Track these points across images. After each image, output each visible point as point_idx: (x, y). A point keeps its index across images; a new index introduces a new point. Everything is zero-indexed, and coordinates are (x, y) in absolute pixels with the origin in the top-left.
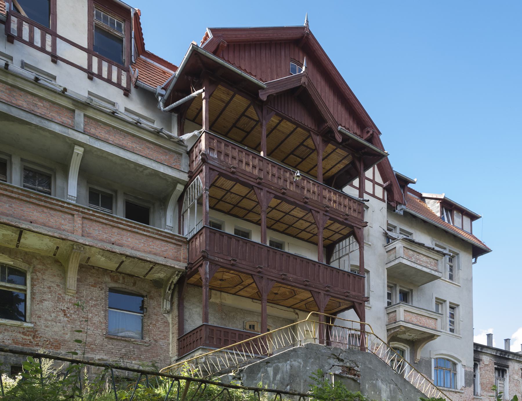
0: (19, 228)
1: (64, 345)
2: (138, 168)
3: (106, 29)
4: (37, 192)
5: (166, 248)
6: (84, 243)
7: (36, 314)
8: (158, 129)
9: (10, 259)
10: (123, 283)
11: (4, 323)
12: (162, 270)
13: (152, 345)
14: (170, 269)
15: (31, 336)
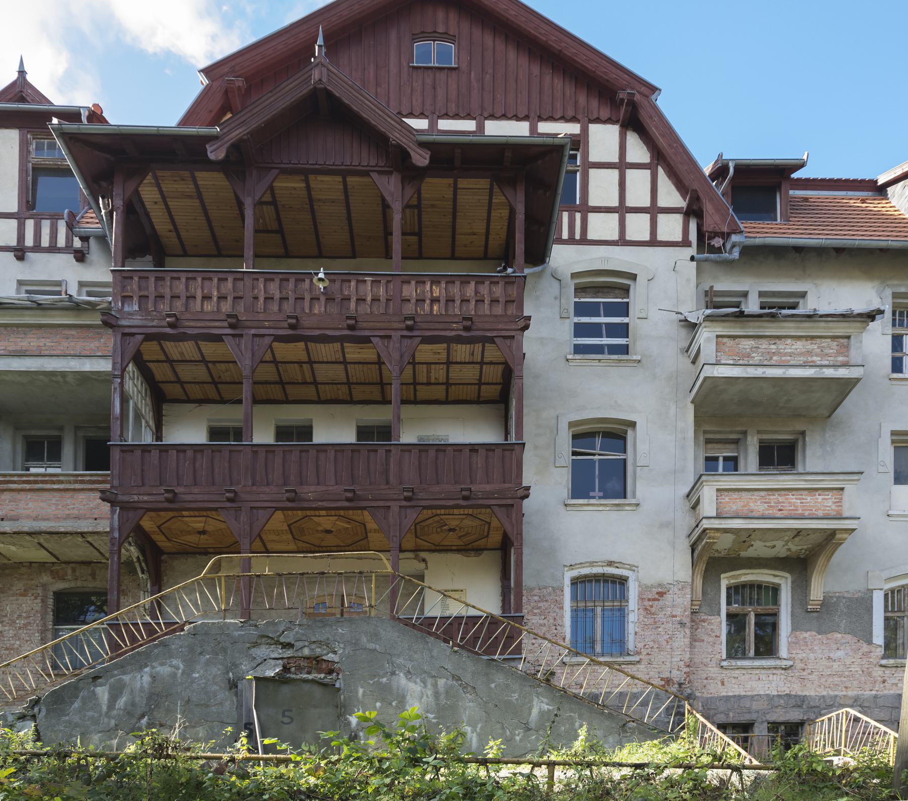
3: (50, 165)
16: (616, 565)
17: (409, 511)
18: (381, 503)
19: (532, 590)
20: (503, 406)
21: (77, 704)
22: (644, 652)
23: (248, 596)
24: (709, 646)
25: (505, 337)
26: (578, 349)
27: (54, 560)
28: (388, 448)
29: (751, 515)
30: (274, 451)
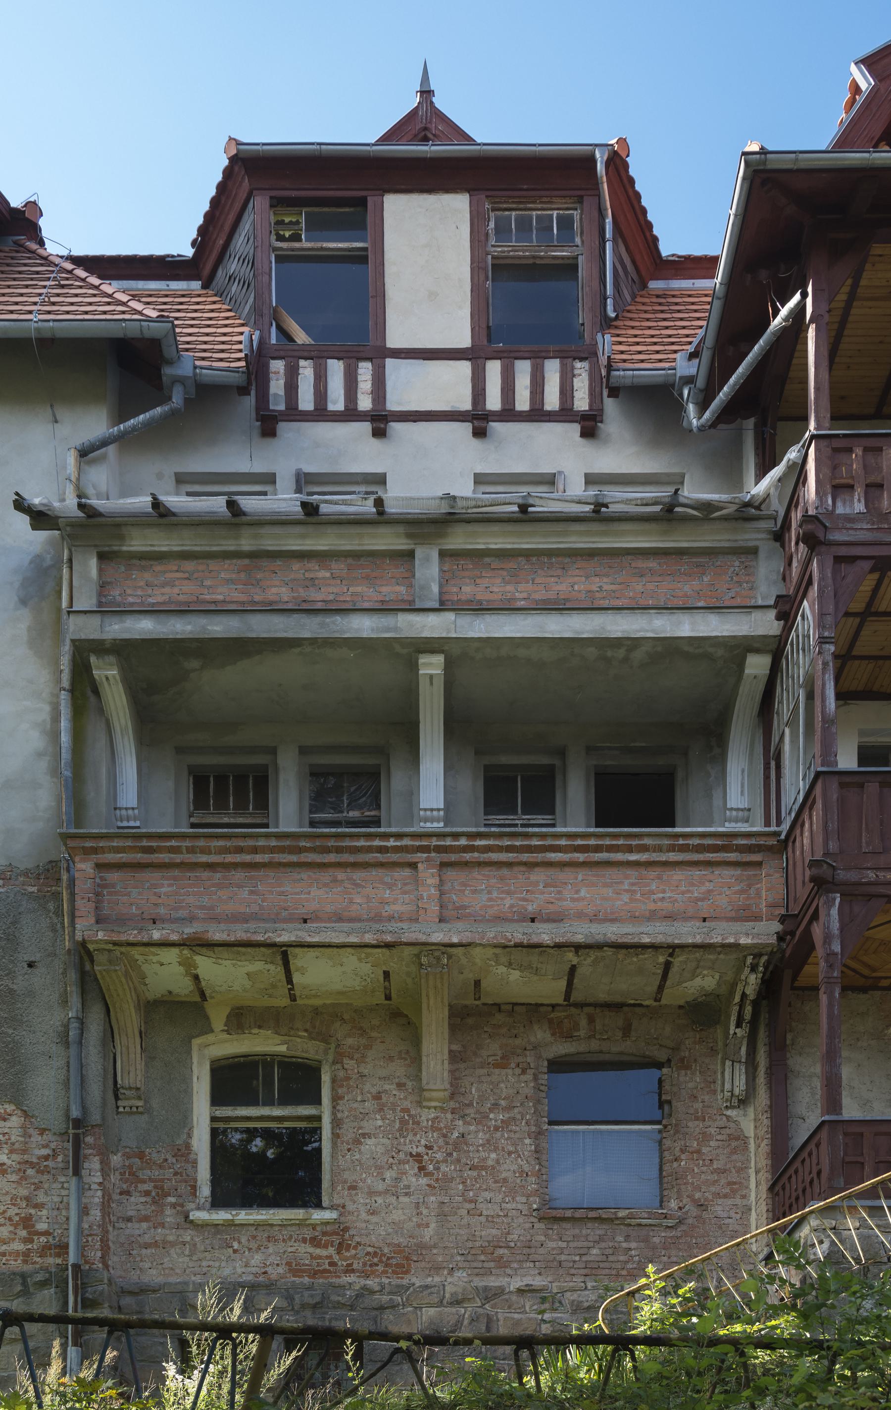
0: (273, 945)
1: (421, 1258)
2: (609, 654)
3: (525, 257)
4: (347, 830)
5: (709, 886)
6: (446, 940)
7: (345, 1182)
8: (663, 500)
9: (278, 1039)
10: (589, 1037)
11: (266, 1220)
12: (702, 964)
13: (690, 1221)
14: (726, 954)
15: (332, 1246)
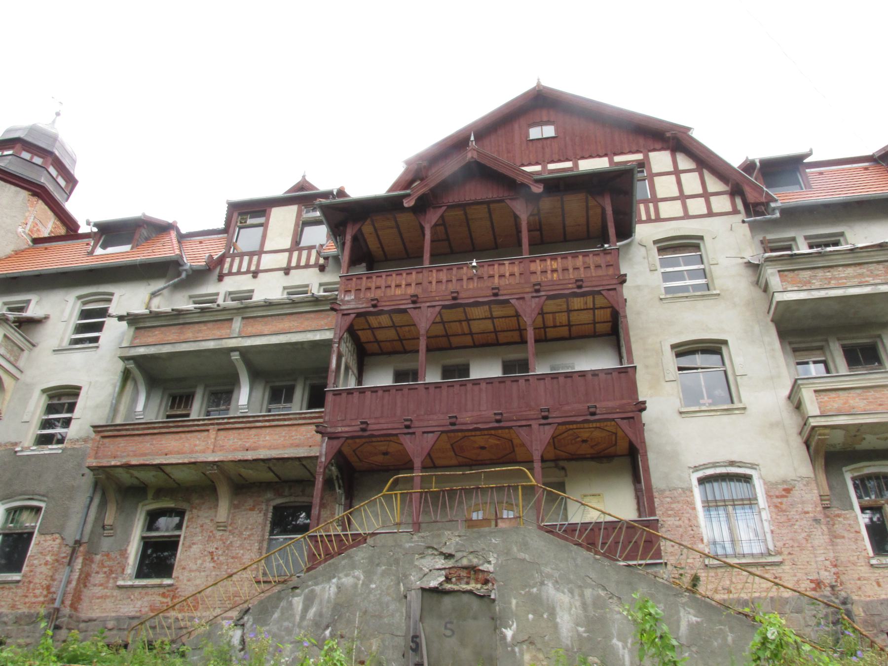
16: (737, 464)
17: (547, 427)
18: (524, 423)
19: (662, 491)
20: (614, 337)
21: (276, 615)
22: (786, 552)
23: (418, 507)
24: (852, 543)
25: (609, 290)
26: (668, 290)
27: (277, 480)
28: (526, 378)
29: (853, 411)
30: (441, 387)
